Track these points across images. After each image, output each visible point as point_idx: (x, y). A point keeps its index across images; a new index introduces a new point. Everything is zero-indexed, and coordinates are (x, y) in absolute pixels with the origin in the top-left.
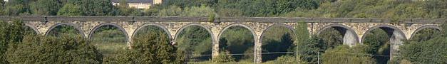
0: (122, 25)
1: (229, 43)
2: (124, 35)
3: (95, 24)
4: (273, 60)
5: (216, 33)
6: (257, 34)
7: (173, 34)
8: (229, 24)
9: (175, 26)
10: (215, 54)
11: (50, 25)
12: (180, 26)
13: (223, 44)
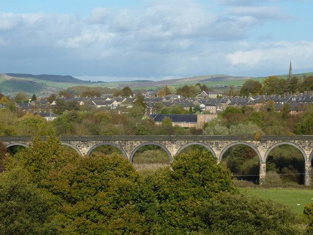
0: (165, 144)
1: (274, 158)
2: (167, 154)
3: (137, 144)
4: (247, 82)
5: (263, 153)
6: (306, 152)
7: (218, 154)
8: (277, 143)
9: (220, 145)
10: (263, 174)
11: (92, 145)
12: (225, 145)
13: (270, 159)
